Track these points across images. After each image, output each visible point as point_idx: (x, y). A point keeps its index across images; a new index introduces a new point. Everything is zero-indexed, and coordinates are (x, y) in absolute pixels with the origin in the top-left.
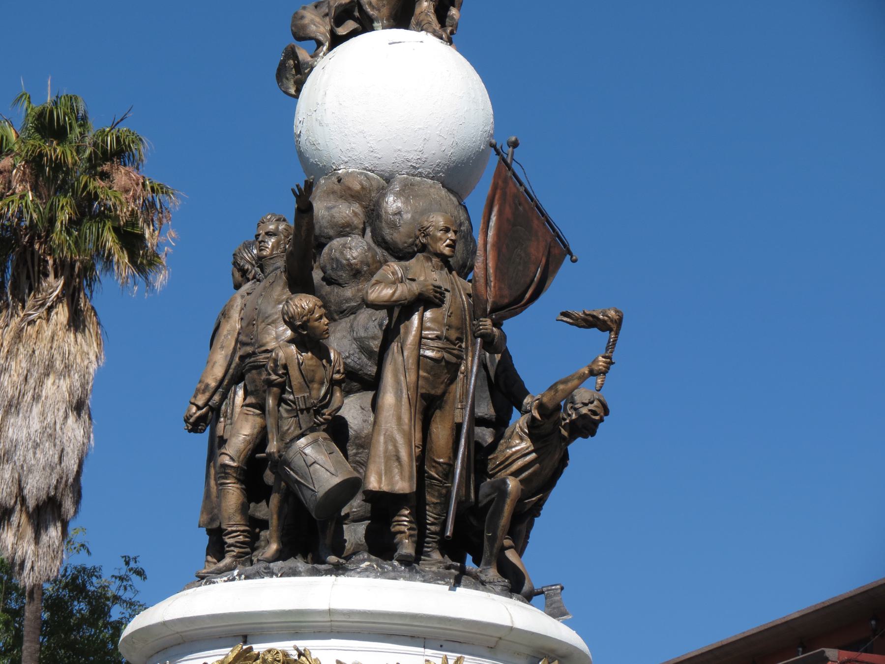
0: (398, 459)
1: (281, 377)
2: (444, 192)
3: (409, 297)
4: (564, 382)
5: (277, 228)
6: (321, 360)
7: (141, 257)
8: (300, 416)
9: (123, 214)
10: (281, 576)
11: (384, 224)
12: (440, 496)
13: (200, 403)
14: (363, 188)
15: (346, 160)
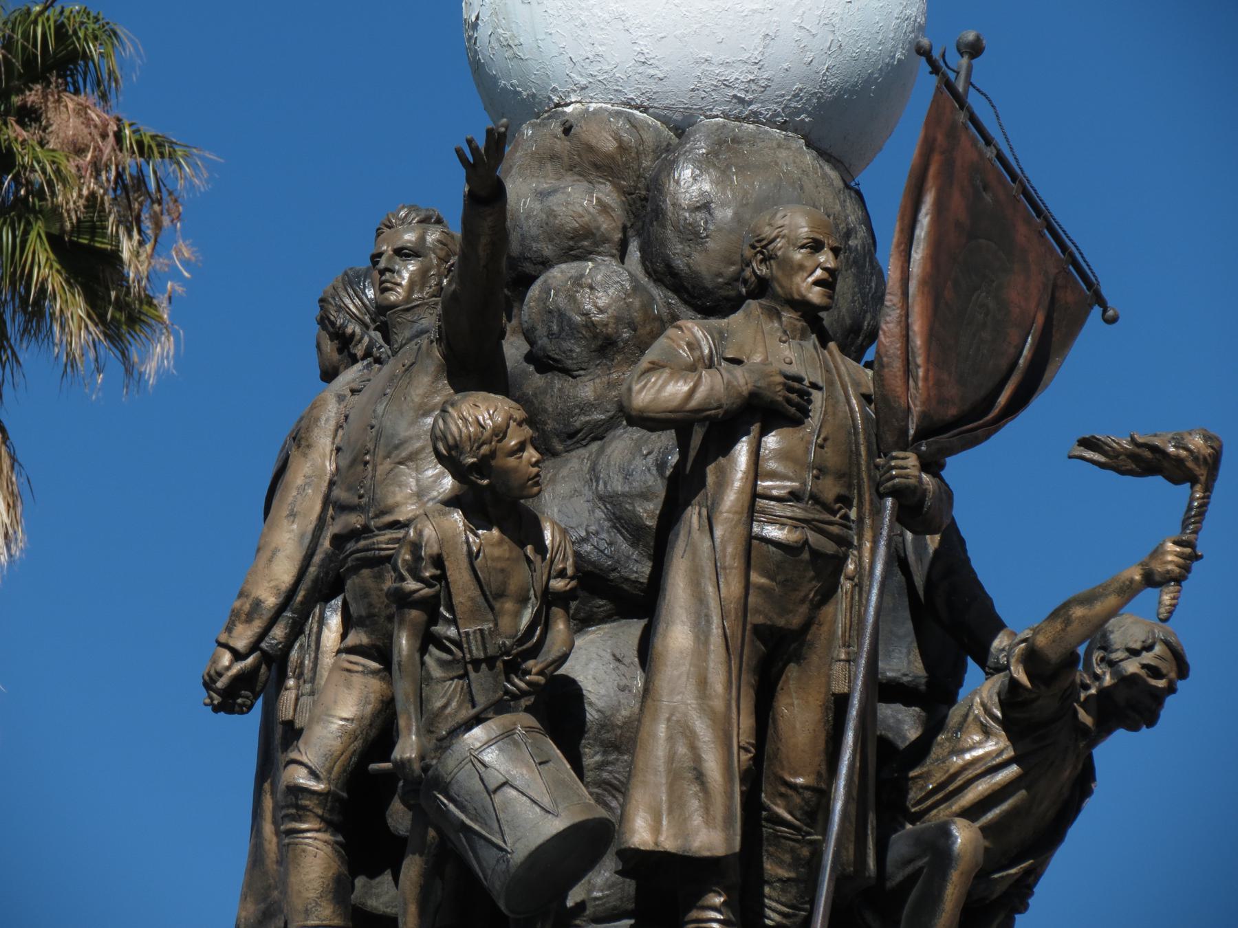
0: (700, 777)
1: (430, 586)
2: (809, 157)
4: (1087, 599)
5: (422, 239)
6: (522, 546)
7: (120, 312)
8: (472, 675)
9: (70, 200)
11: (669, 232)
12: (796, 862)
13: (241, 644)
14: (622, 147)
15: (583, 82)
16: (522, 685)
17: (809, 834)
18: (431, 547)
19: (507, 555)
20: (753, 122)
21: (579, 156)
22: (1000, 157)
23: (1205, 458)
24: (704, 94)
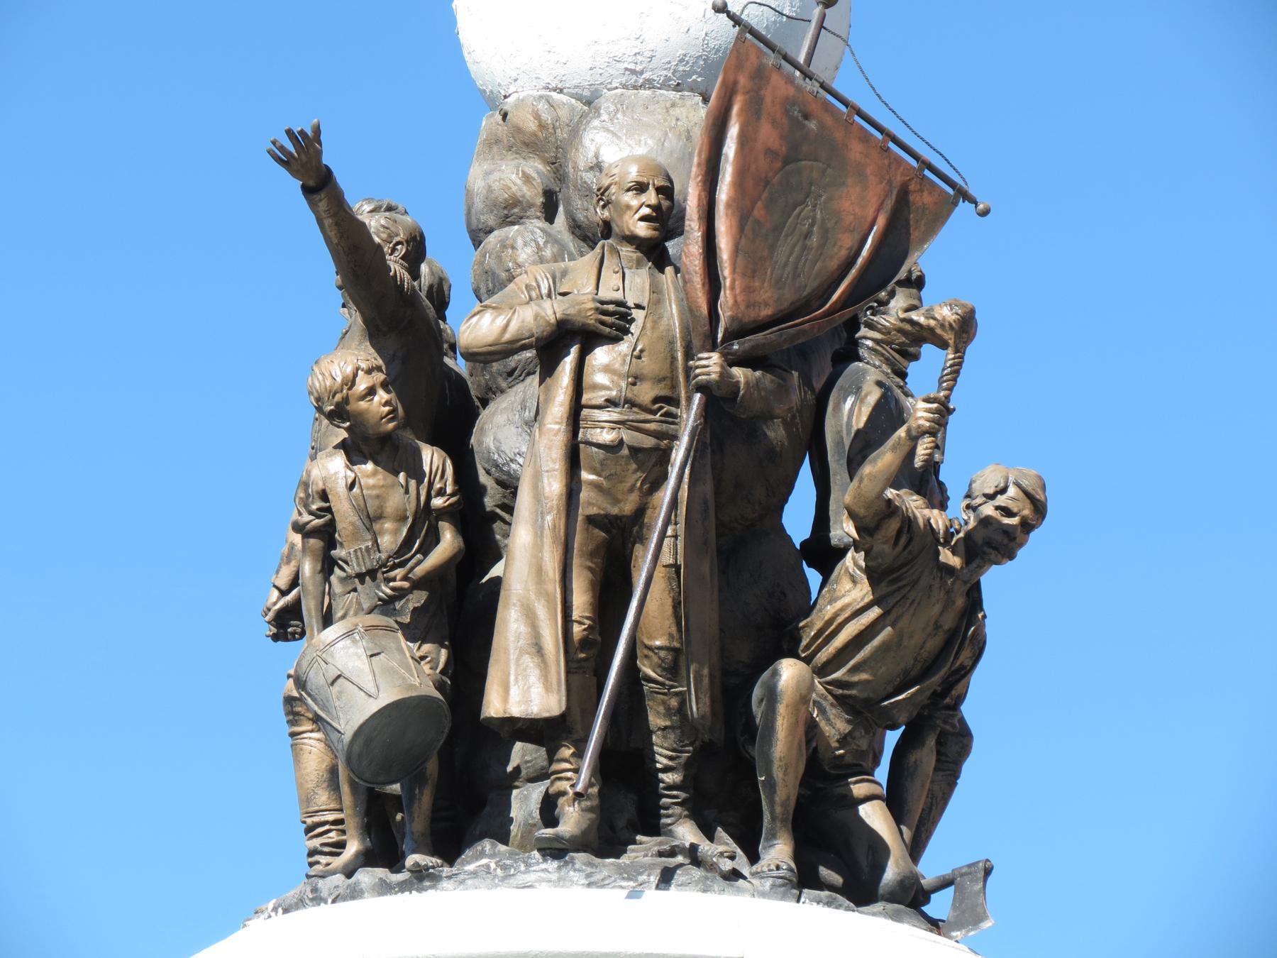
0: (539, 650)
1: (319, 517)
3: (537, 331)
6: (396, 474)
8: (359, 587)
10: (334, 901)
14: (542, 126)
15: (514, 75)
16: (388, 591)
17: (673, 687)
22: (822, 86)
23: (951, 325)
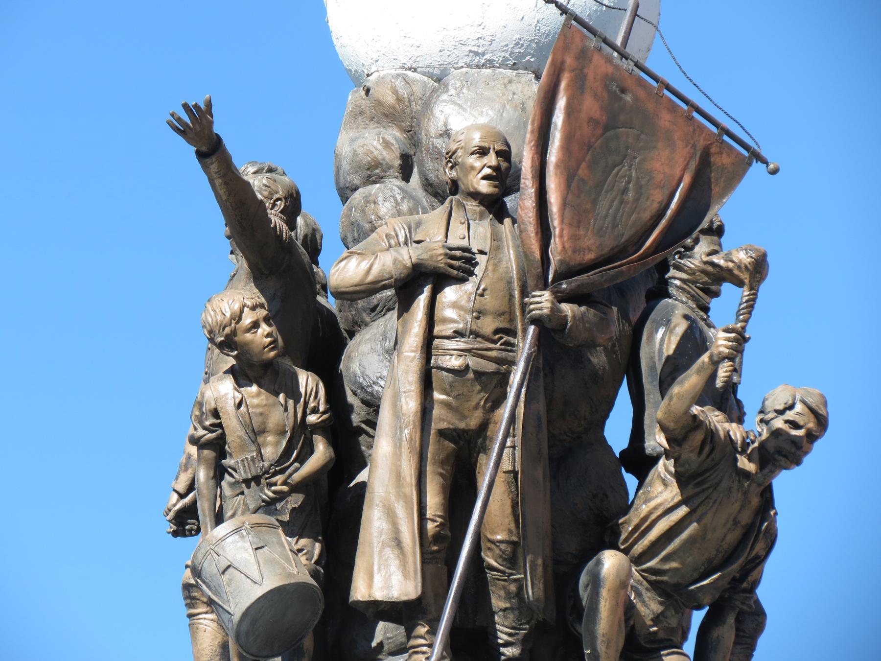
0: (398, 543)
1: (211, 432)
8: (246, 491)
14: (399, 100)
15: (375, 57)
16: (271, 494)
17: (512, 574)
18: (210, 404)
19: (264, 402)
20: (490, 67)
21: (375, 109)
23: (746, 267)
24: (448, 53)
